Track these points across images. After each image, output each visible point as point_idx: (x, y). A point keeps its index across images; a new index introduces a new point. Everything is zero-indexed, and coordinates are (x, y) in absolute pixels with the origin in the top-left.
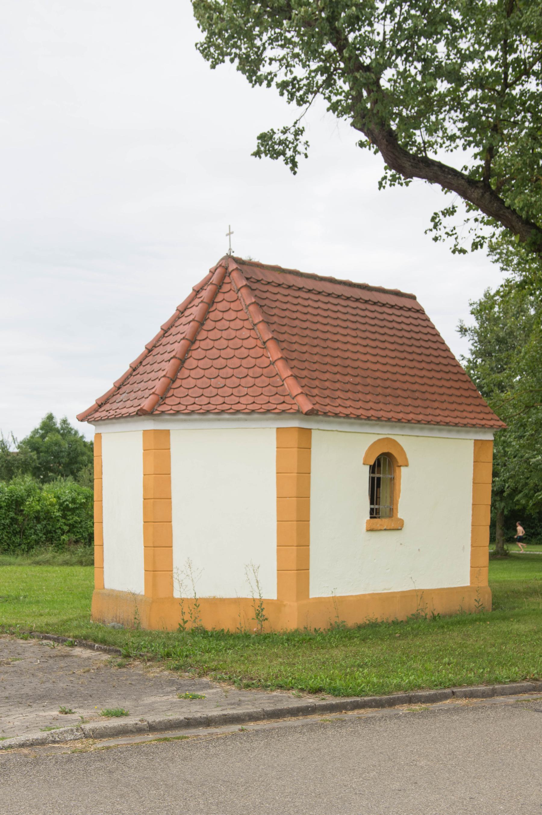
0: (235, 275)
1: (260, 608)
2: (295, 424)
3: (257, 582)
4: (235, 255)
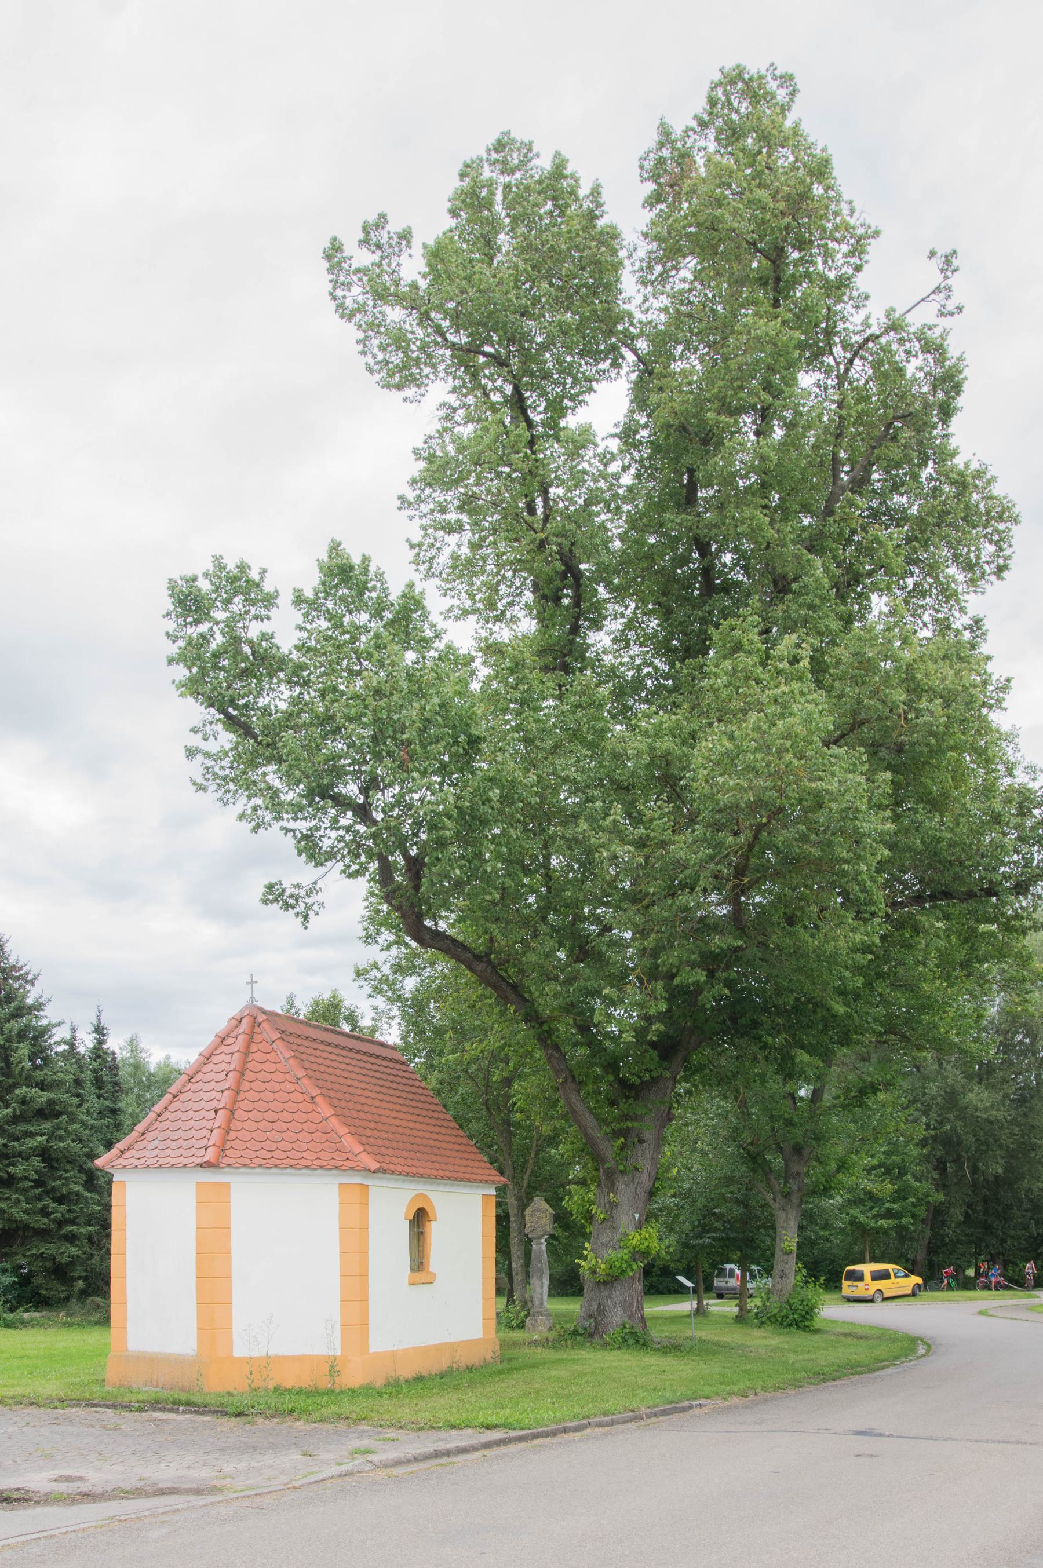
0: (265, 1025)
1: (333, 1367)
2: (357, 1180)
3: (872, 1456)
4: (259, 1004)
